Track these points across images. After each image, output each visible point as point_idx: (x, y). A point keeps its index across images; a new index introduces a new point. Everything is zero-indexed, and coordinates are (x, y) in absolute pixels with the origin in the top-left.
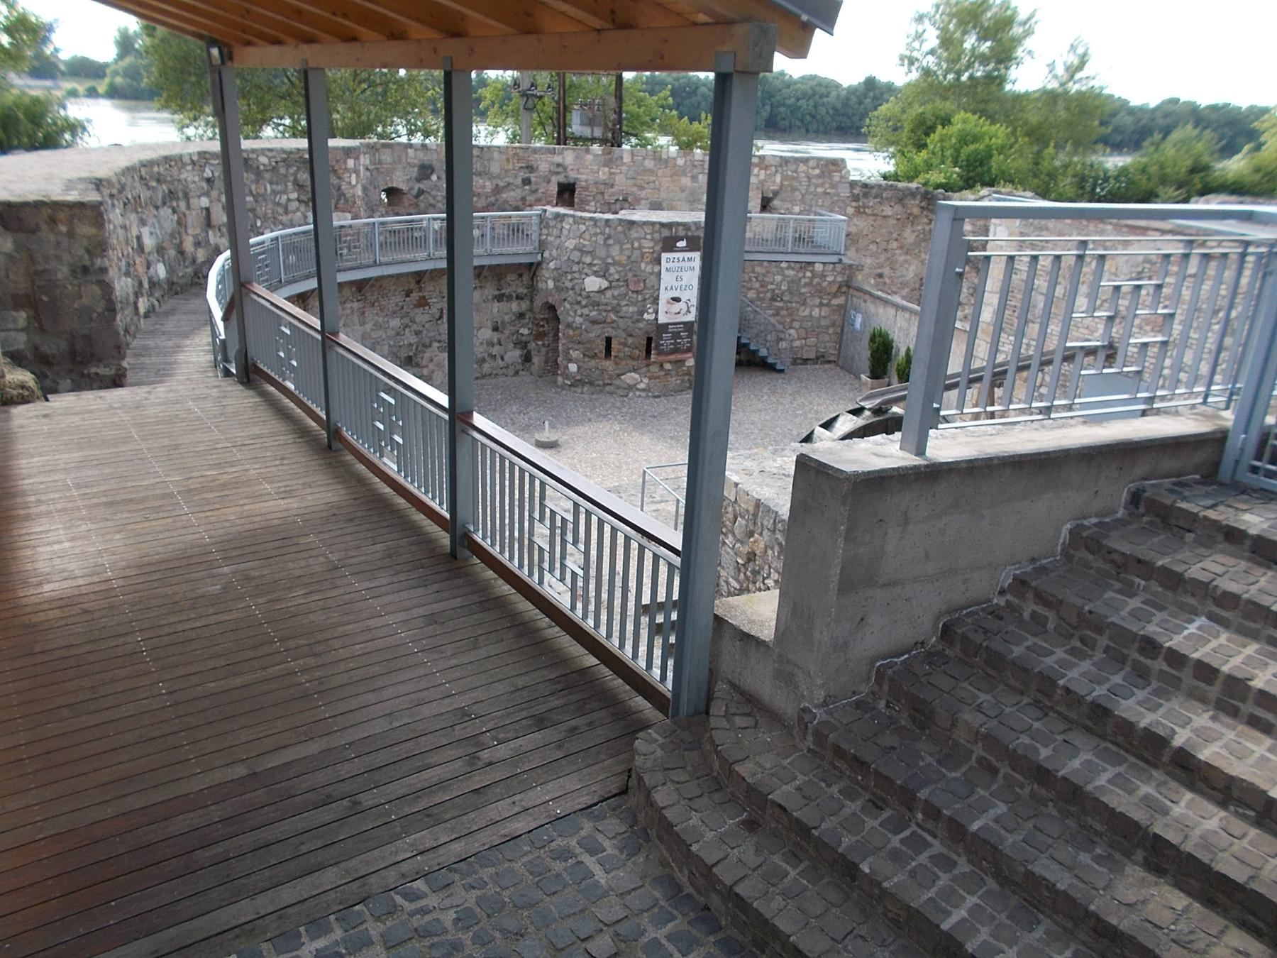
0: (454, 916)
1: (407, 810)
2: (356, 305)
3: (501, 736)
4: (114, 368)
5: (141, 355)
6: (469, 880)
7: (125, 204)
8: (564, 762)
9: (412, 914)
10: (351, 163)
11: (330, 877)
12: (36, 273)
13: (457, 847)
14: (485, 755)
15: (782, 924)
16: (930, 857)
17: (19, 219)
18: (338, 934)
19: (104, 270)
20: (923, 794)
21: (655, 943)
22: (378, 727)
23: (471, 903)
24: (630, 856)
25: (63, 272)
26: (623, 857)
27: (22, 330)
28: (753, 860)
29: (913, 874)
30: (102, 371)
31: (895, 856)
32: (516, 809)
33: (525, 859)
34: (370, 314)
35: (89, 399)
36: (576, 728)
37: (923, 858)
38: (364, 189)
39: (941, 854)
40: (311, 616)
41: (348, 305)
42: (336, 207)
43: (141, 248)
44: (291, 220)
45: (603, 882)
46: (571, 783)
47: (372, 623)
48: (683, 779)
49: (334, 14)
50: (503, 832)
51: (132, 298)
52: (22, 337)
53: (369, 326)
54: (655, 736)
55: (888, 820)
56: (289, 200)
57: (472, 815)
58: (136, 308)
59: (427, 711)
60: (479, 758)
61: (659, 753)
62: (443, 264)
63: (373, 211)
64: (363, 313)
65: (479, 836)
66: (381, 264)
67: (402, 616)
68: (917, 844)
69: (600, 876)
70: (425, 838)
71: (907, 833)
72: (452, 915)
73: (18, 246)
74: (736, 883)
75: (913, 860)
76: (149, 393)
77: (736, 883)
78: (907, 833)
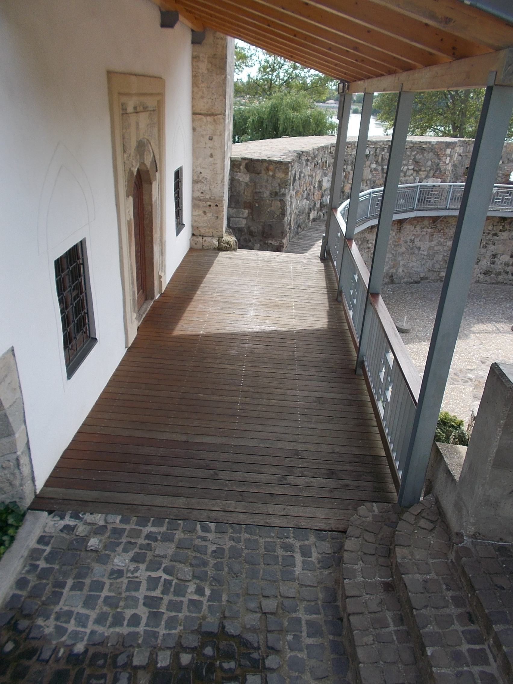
0: (215, 549)
1: (235, 488)
2: (429, 230)
3: (305, 473)
4: (279, 242)
5: (301, 239)
6: (235, 535)
7: (315, 165)
8: (327, 500)
9: (198, 537)
10: (448, 151)
11: (180, 502)
12: (256, 193)
13: (242, 517)
14: (290, 479)
15: (361, 653)
16: (483, 672)
17: (254, 167)
18: (163, 529)
19: (284, 195)
20: (497, 628)
21: (298, 620)
22: (252, 443)
23: (226, 547)
24: (322, 567)
25: (266, 194)
26: (318, 566)
27: (245, 218)
28: (374, 606)
29: (459, 675)
30: (274, 243)
31: (457, 657)
32: (282, 513)
33: (268, 540)
34: (436, 236)
35: (267, 254)
36: (347, 486)
37: (476, 669)
38: (454, 166)
39: (492, 675)
40: (265, 379)
41: (425, 230)
42: (433, 175)
43: (320, 187)
44: (407, 180)
45: (297, 573)
46: (321, 513)
47: (288, 392)
48: (370, 540)
49: (356, 60)
50: (268, 521)
51: (307, 210)
52: (244, 222)
53: (433, 243)
54: (375, 508)
55: (470, 631)
56: (408, 169)
57: (260, 505)
58: (309, 216)
59: (280, 445)
60: (286, 479)
61: (370, 519)
62: (456, 213)
63: (457, 179)
64: (433, 235)
65: (256, 517)
66: (449, 209)
67: (306, 393)
68: (479, 658)
69: (298, 569)
70: (231, 505)
71: (477, 647)
72: (214, 548)
73: (251, 180)
74: (354, 614)
75: (468, 666)
76: (278, 256)
77: (354, 614)
78: (477, 647)
